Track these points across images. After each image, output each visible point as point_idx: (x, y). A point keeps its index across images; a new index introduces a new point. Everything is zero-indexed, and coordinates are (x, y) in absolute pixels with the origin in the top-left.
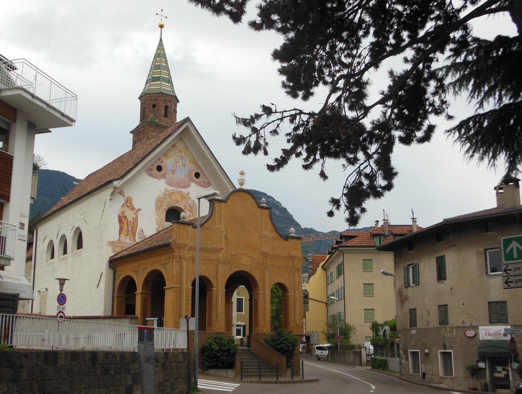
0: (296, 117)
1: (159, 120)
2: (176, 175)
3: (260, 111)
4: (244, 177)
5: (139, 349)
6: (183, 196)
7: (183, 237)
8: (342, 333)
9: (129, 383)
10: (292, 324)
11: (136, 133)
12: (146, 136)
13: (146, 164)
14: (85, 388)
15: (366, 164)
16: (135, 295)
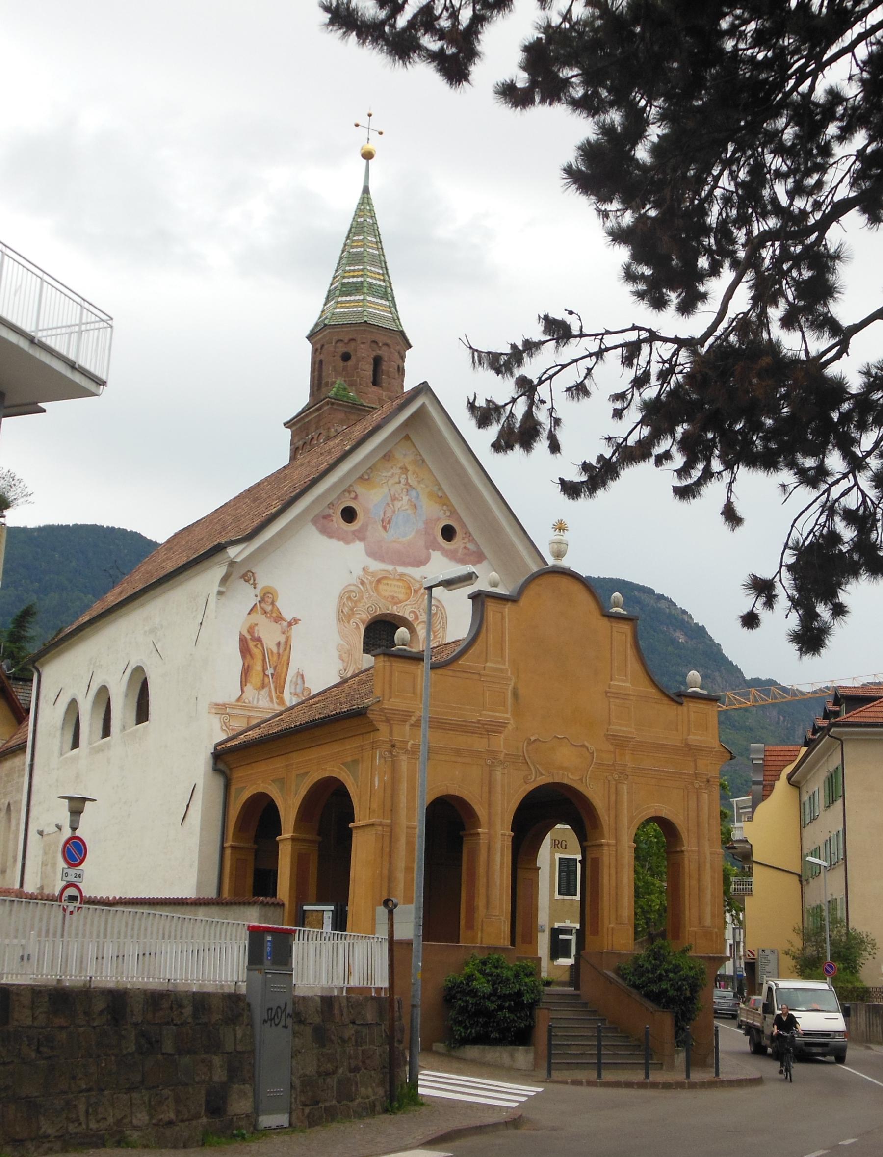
0: (639, 349)
1: (358, 392)
2: (392, 531)
3: (537, 333)
4: (566, 536)
5: (248, 987)
6: (409, 588)
7: (414, 694)
8: (837, 956)
9: (216, 1079)
10: (691, 928)
11: (299, 425)
12: (324, 433)
13: (313, 502)
14: (89, 1090)
15: (845, 484)
16: (277, 844)
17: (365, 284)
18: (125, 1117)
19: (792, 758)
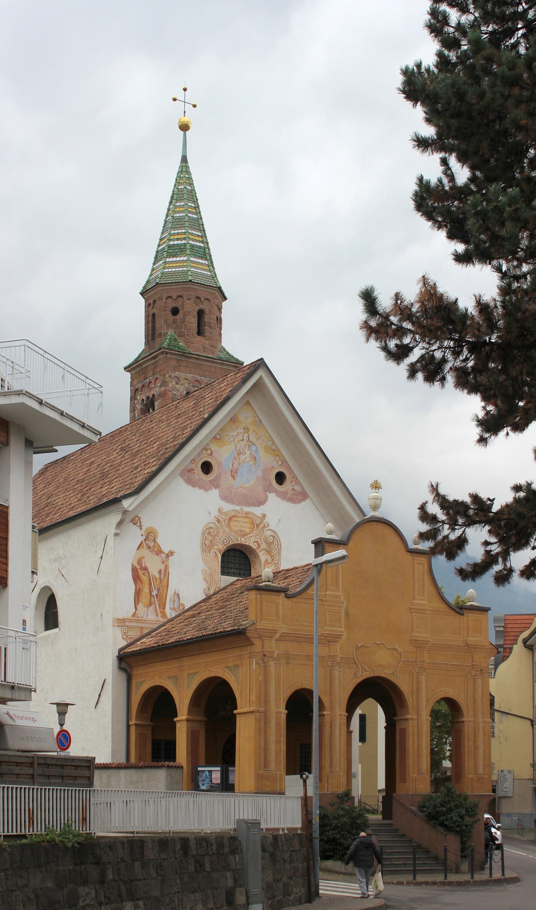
1: (186, 342)
2: (238, 479)
12: (161, 378)
14: (178, 892)
16: (174, 725)
17: (188, 247)
18: (193, 906)
19: (527, 625)
